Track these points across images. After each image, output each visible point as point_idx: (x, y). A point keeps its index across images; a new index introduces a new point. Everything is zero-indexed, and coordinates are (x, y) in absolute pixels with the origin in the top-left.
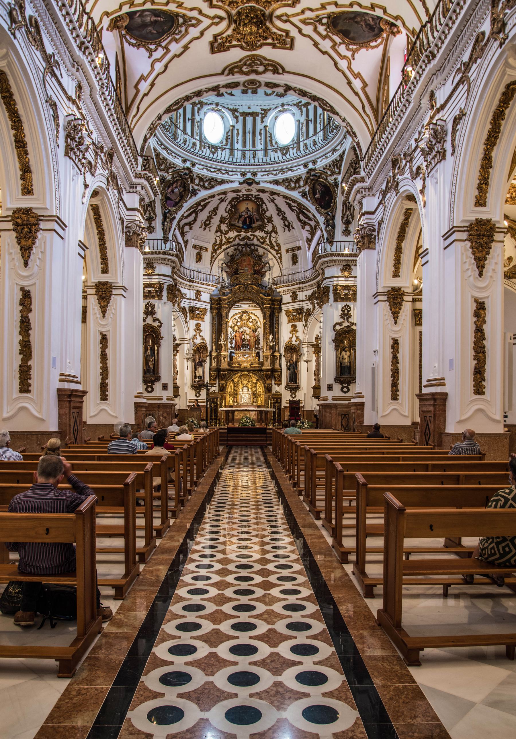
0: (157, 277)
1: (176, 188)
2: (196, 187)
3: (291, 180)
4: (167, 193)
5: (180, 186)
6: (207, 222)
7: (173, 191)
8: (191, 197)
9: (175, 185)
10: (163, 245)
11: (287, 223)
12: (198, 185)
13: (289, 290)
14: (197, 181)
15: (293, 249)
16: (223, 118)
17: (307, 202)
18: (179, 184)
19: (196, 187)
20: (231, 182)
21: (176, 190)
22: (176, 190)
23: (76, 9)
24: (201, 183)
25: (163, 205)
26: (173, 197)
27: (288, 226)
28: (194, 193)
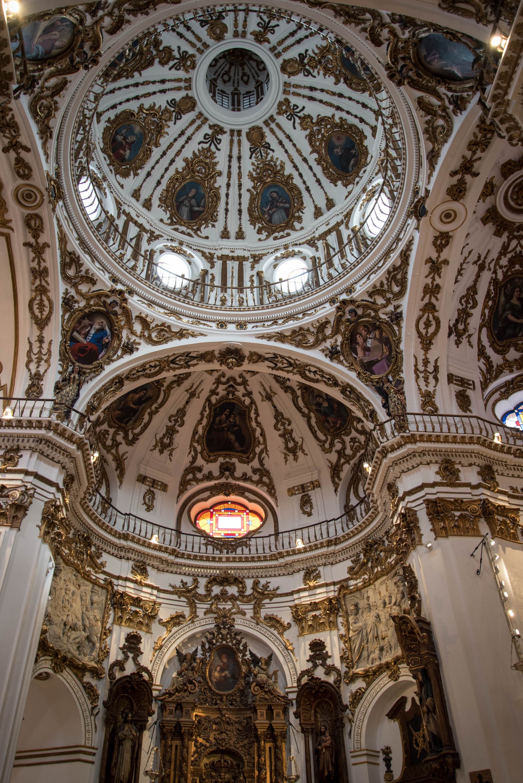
0: (149, 590)
1: (365, 340)
2: (390, 308)
3: (308, 330)
4: (361, 361)
5: (369, 332)
6: (461, 327)
7: (366, 349)
8: (400, 327)
9: (360, 340)
10: (203, 548)
11: (461, 327)
12: (388, 301)
13: (435, 452)
14: (380, 301)
15: (303, 487)
16: (190, 263)
17: (339, 367)
18: (364, 333)
19: (390, 308)
20: (410, 243)
21: (369, 343)
22: (369, 343)
23: (94, 503)
24: (389, 295)
25: (367, 381)
26: (375, 355)
27: (459, 335)
28: (397, 317)
